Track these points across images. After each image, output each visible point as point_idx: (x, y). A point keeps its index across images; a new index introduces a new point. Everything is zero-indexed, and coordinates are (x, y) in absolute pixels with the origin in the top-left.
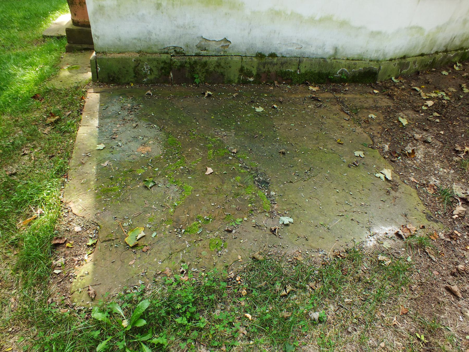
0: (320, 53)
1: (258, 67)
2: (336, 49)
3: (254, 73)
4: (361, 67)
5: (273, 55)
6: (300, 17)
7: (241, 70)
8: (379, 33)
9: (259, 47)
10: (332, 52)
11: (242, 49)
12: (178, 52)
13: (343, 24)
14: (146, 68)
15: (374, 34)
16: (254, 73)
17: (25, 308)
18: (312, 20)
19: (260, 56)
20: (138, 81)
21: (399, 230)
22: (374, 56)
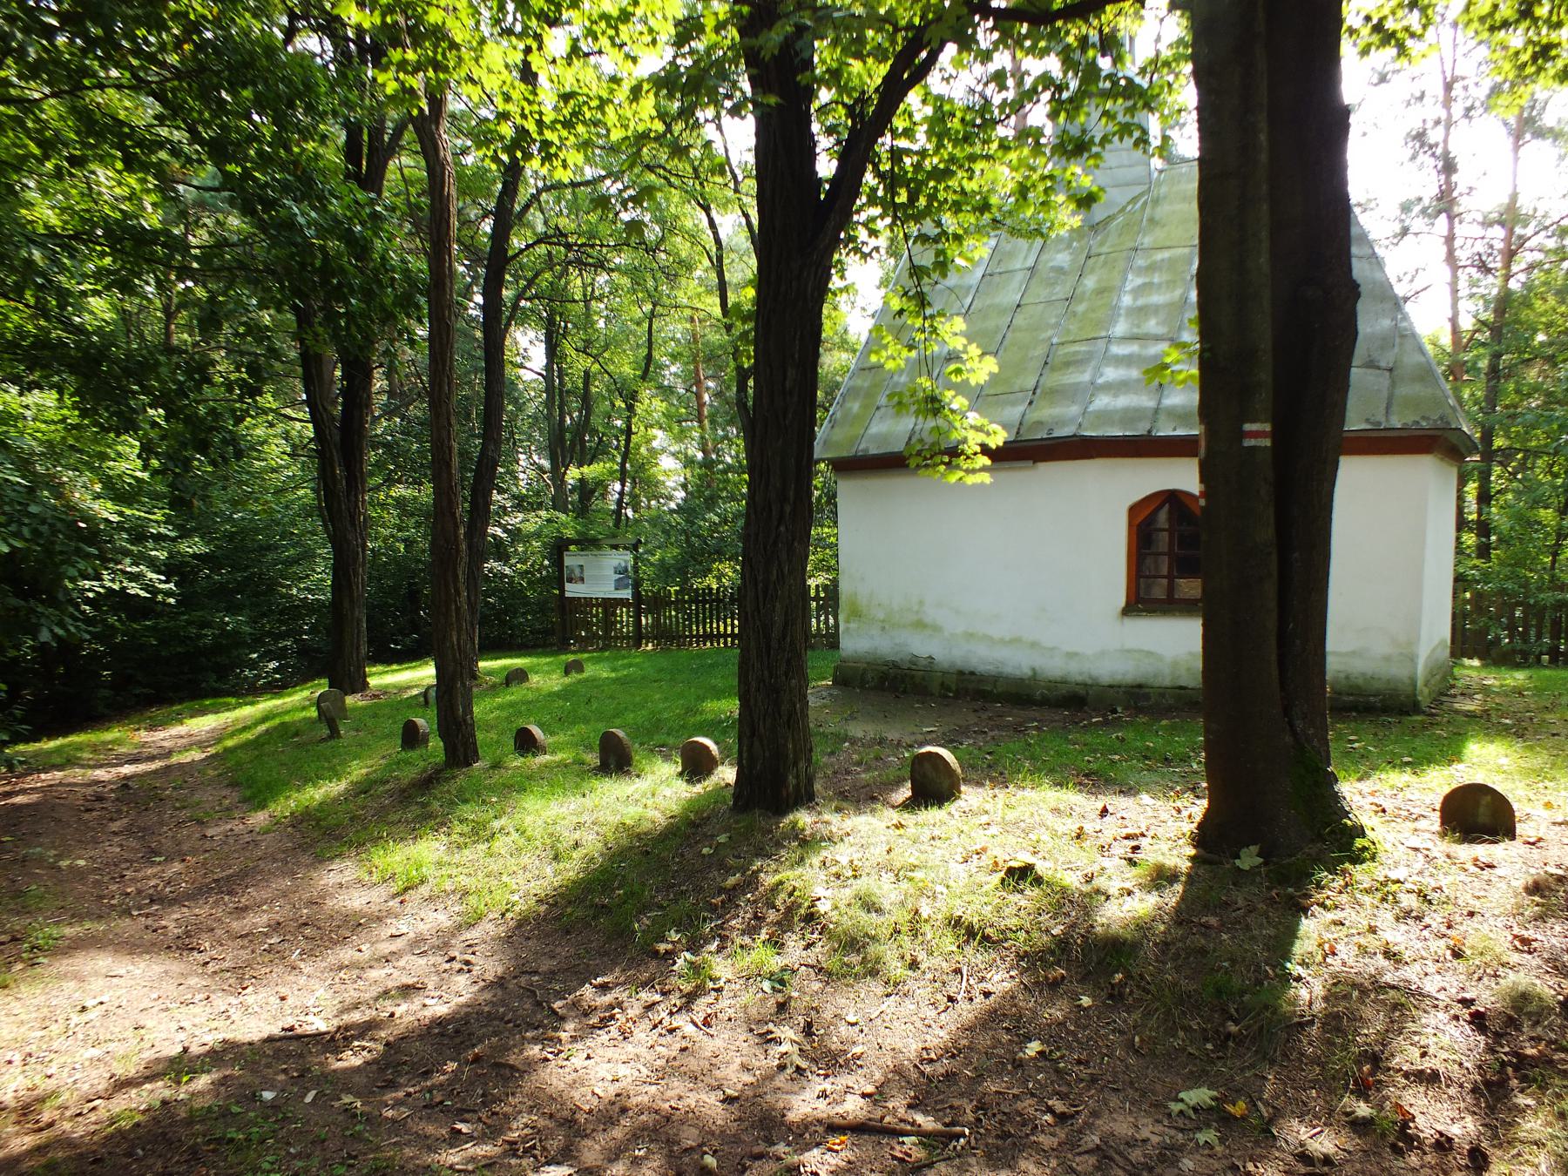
0: (1018, 673)
1: (535, 86)
2: (1033, 670)
3: (954, 687)
4: (1063, 690)
5: (972, 673)
6: (991, 639)
7: (942, 684)
8: (1076, 654)
9: (960, 664)
10: (1030, 673)
11: (946, 665)
12: (895, 665)
13: (1034, 645)
14: (869, 676)
15: (1071, 655)
16: (954, 687)
17: (1191, 1072)
18: (1002, 642)
19: (961, 673)
20: (862, 687)
21: (585, 675)
22: (1079, 679)
